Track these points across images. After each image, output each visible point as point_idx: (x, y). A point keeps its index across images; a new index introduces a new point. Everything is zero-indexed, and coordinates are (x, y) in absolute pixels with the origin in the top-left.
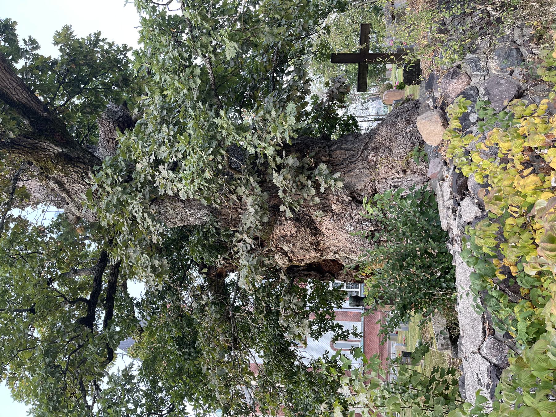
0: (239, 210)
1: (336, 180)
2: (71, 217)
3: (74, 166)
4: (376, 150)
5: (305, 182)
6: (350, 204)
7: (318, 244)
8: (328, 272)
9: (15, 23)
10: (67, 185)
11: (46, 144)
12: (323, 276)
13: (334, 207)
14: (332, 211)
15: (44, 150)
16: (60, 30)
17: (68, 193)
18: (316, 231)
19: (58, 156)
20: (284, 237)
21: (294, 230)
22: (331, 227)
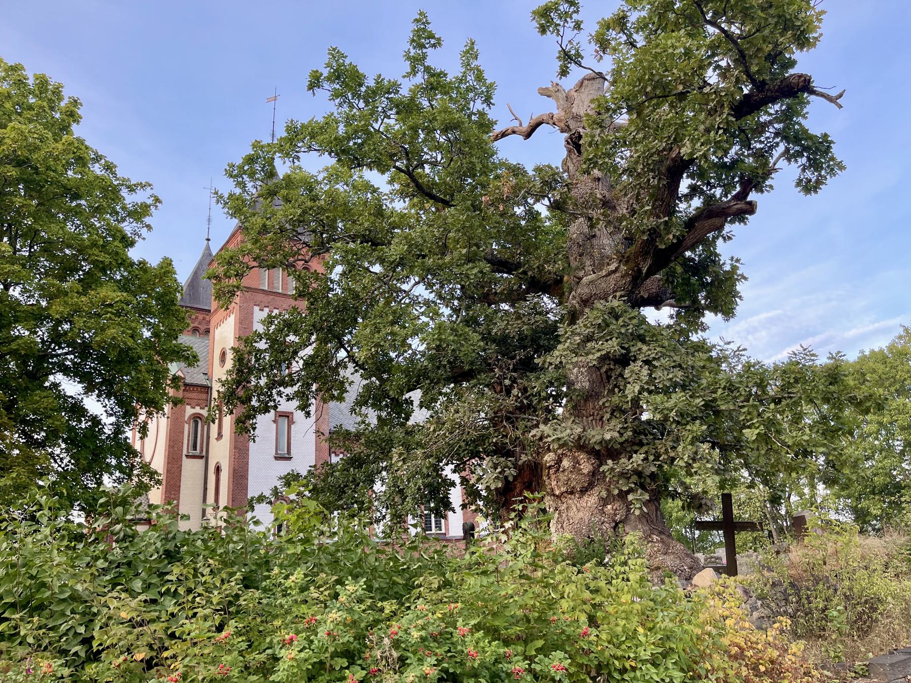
0: (591, 418)
1: (640, 508)
2: (581, 274)
3: (630, 282)
4: (662, 541)
5: (631, 481)
6: (614, 521)
7: (572, 493)
8: (506, 499)
9: (745, 224)
10: (613, 276)
11: (649, 262)
12: (501, 494)
13: (609, 507)
14: (605, 505)
15: (644, 260)
16: (737, 223)
17: (606, 276)
18: (584, 491)
19: (640, 271)
20: (578, 462)
21: (585, 471)
22: (589, 504)
